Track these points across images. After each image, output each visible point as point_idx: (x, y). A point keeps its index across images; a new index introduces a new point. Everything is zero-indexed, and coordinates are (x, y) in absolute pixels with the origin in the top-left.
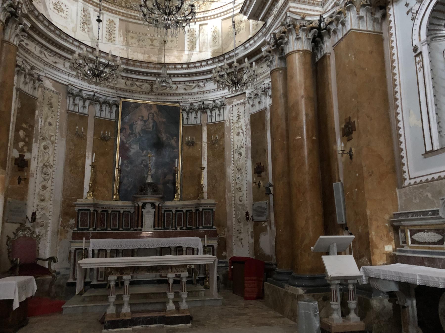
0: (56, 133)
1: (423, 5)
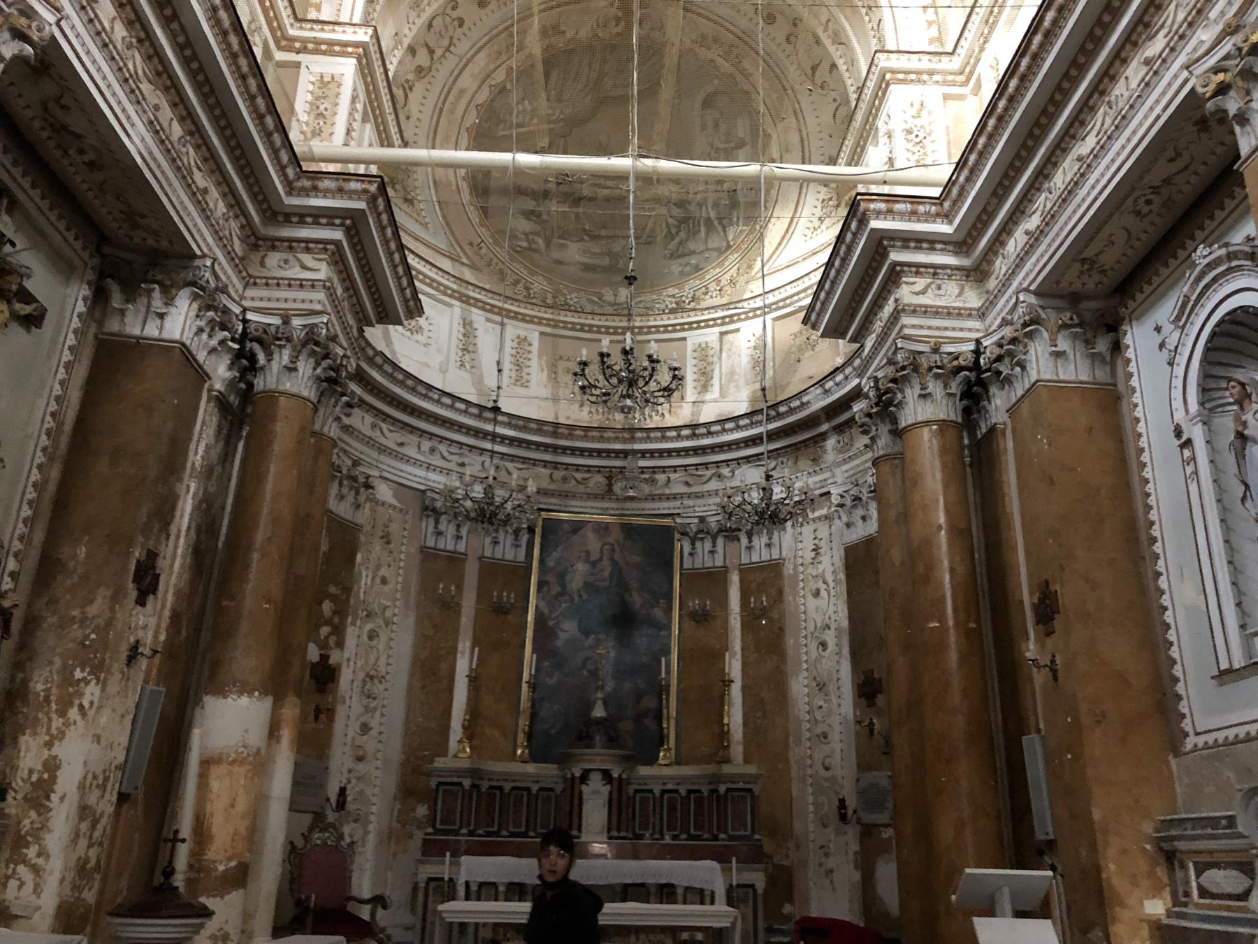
0: (396, 600)
1: (1187, 335)
